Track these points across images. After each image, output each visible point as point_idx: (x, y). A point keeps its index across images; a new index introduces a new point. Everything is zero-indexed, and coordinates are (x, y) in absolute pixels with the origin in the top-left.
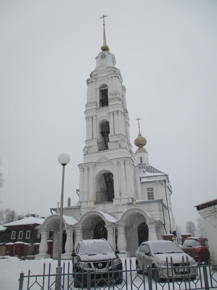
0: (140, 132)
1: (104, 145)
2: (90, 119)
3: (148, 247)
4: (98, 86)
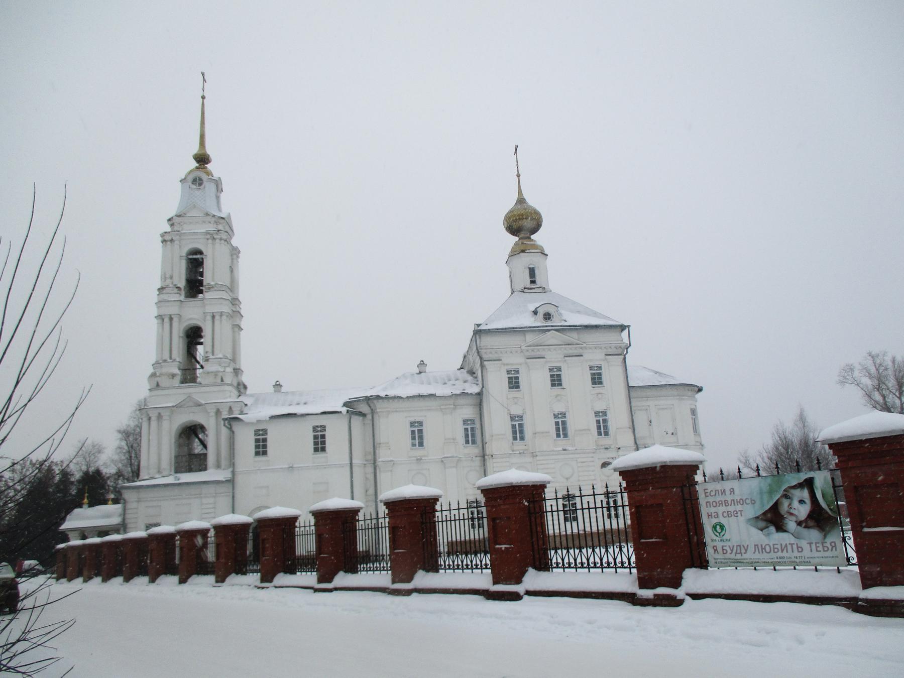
1: (189, 375)
2: (167, 320)
3: (769, 548)
4: (184, 252)
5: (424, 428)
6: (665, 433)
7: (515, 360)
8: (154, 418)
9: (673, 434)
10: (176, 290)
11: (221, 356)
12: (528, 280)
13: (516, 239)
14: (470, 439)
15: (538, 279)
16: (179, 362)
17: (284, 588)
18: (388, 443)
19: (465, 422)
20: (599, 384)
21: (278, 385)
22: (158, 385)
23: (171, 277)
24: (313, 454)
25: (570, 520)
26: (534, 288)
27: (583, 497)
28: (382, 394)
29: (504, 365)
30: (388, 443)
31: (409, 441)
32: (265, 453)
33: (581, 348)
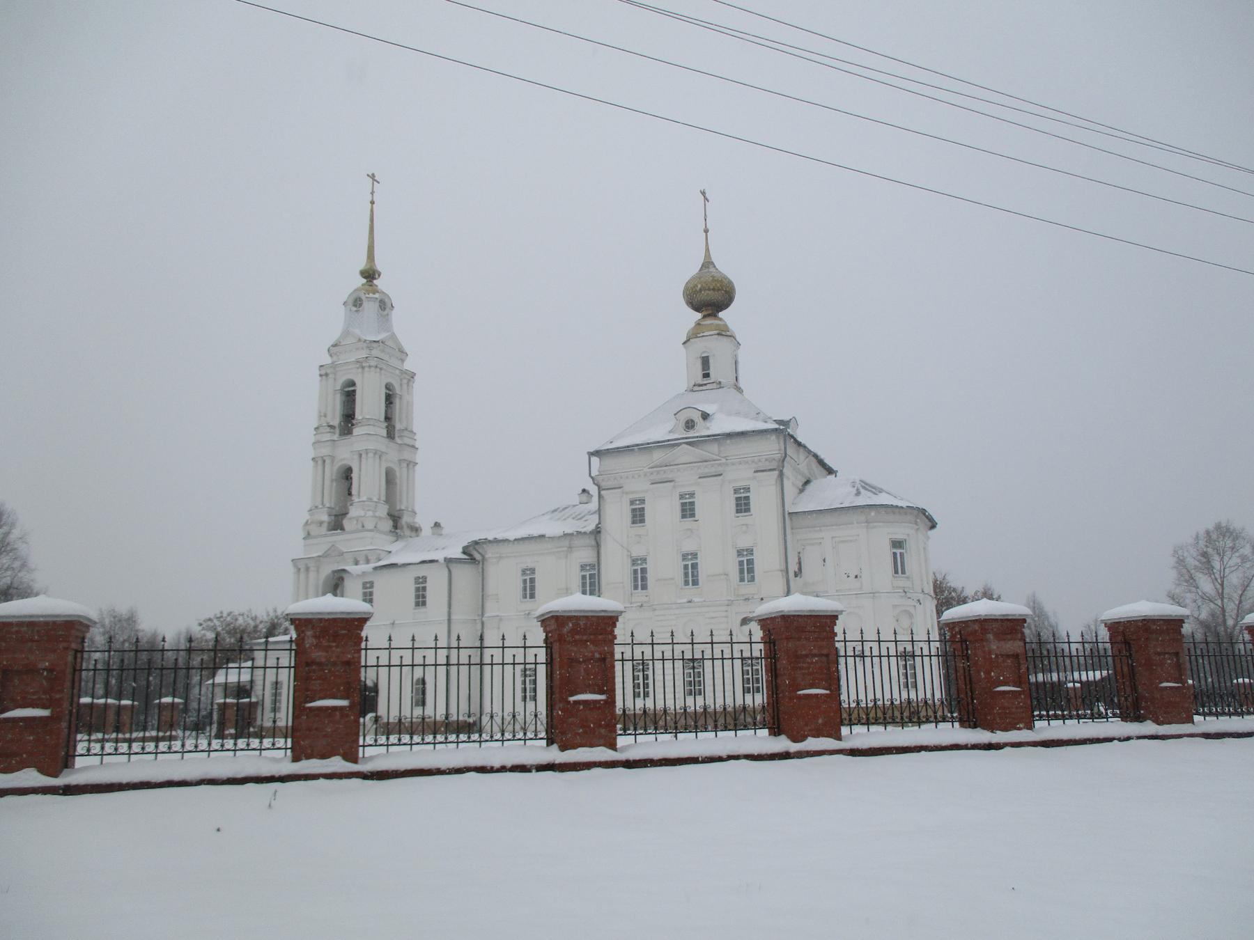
0: (707, 250)
2: (320, 462)
5: (537, 576)
6: (846, 575)
7: (638, 487)
8: (302, 570)
9: (856, 577)
10: (328, 429)
11: (364, 498)
12: (700, 373)
13: (699, 316)
14: (640, 583)
15: (712, 372)
16: (328, 508)
17: (1226, 740)
18: (497, 595)
19: (583, 567)
20: (745, 512)
21: (437, 525)
22: (309, 534)
23: (325, 416)
24: (415, 609)
25: (755, 689)
26: (705, 384)
27: (715, 661)
28: (491, 538)
29: (627, 493)
30: (497, 595)
31: (520, 592)
32: (424, 604)
33: (720, 465)
